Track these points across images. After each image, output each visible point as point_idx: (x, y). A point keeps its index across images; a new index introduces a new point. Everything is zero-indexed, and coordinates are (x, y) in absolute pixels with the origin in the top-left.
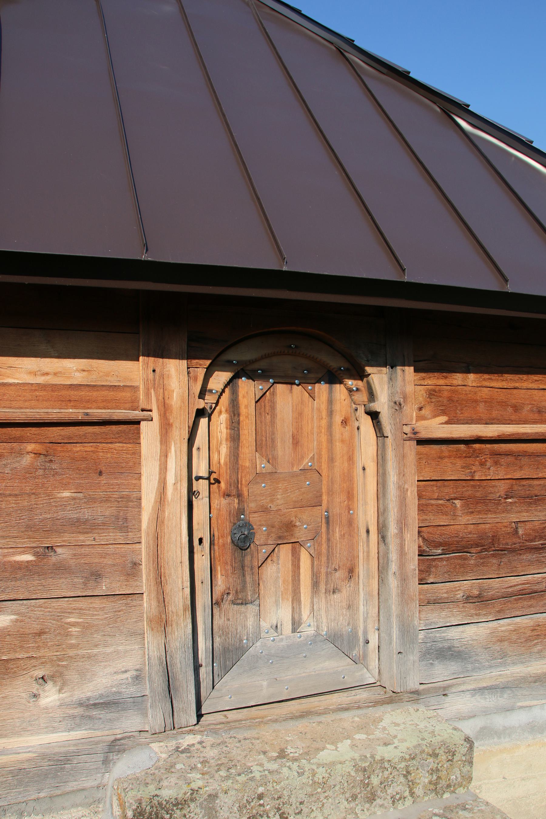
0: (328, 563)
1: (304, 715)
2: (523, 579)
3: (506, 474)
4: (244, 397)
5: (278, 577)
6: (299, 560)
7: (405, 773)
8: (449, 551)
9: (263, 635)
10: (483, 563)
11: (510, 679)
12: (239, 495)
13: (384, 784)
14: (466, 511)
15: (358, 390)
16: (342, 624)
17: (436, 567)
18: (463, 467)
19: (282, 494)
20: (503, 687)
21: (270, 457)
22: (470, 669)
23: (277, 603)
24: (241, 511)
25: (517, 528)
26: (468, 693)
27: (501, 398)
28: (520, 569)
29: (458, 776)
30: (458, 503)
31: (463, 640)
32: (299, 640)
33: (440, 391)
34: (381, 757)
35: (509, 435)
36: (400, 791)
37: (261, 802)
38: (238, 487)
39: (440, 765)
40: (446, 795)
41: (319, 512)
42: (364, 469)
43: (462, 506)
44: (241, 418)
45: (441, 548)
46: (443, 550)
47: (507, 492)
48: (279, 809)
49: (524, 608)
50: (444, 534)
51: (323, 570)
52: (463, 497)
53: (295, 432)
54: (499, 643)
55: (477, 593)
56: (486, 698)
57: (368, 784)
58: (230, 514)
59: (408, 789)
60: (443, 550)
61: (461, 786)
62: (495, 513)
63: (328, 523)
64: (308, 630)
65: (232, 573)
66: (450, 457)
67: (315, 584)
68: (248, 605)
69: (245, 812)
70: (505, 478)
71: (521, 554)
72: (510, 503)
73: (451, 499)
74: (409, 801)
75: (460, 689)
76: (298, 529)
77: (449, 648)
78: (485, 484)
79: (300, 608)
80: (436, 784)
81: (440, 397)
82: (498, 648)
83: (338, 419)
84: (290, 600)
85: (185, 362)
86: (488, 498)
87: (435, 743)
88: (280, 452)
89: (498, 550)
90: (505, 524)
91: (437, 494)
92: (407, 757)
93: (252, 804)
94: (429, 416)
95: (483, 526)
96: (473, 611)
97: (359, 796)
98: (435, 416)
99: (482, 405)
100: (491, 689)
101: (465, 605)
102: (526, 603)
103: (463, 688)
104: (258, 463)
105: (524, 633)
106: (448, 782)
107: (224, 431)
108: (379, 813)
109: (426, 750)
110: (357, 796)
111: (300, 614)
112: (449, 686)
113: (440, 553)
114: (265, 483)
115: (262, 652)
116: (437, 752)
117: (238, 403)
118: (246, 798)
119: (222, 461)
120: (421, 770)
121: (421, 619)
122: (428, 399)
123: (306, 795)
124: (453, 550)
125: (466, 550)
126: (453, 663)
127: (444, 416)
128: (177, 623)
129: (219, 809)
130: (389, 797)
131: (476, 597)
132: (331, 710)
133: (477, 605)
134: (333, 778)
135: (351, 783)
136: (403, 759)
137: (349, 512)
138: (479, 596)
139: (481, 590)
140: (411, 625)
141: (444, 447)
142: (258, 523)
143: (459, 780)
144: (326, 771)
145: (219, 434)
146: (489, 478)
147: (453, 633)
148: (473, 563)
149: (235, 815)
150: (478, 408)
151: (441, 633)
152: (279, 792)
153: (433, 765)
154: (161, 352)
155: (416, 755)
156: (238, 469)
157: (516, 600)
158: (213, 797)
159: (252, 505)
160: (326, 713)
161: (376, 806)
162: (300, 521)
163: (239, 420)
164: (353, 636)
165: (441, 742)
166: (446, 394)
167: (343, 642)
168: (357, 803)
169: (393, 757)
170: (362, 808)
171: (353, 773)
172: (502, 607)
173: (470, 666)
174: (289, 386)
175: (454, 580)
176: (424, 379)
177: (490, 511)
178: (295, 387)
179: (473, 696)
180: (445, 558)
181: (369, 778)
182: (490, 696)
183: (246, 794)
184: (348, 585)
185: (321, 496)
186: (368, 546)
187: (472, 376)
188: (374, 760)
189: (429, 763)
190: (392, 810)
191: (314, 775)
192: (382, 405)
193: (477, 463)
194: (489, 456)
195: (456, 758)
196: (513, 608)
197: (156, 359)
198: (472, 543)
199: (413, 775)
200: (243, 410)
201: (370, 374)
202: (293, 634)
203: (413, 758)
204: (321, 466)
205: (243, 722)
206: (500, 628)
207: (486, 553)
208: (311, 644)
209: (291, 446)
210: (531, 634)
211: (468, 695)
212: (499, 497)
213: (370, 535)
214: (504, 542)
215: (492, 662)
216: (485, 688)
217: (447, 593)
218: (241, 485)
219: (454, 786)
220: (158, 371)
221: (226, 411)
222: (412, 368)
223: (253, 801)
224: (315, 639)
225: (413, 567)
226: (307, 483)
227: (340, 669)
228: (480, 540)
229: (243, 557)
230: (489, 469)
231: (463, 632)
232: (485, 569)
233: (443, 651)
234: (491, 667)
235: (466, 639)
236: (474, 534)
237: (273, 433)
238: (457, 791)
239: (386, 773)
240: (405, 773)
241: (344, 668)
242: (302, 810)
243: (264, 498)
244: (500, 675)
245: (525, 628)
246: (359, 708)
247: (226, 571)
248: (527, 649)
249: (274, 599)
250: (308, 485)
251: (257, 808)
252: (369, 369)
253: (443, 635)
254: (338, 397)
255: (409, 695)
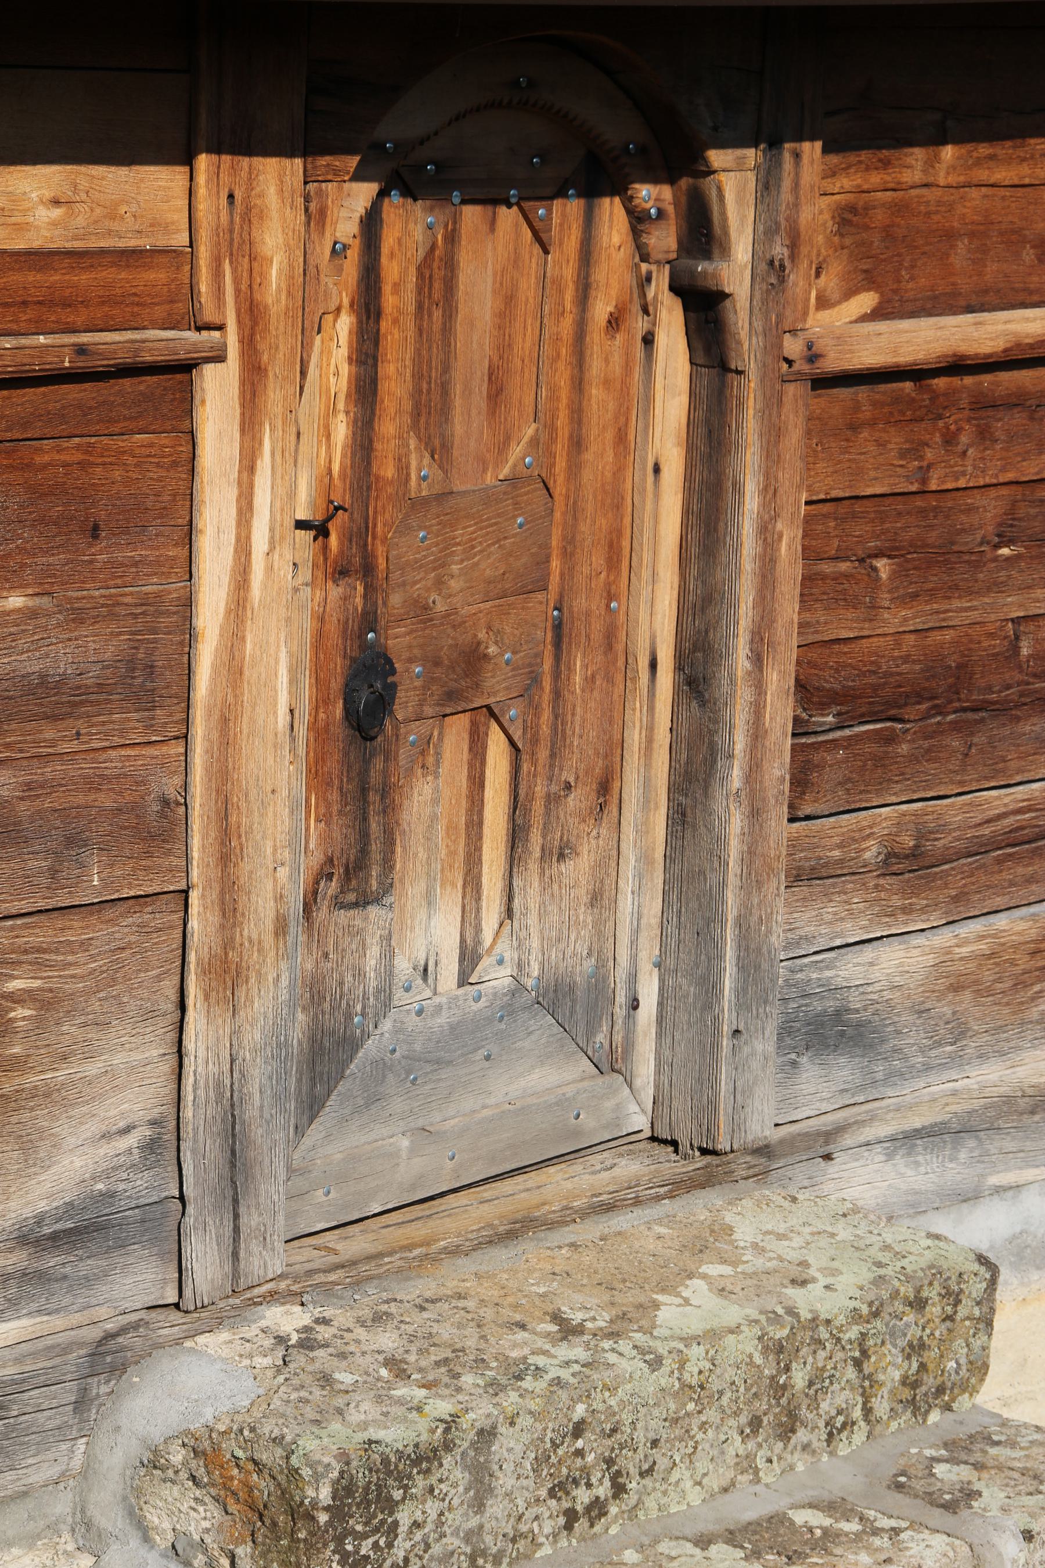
0: (552, 766)
1: (518, 1229)
2: (1020, 797)
3: (1003, 469)
4: (392, 255)
5: (434, 818)
6: (483, 763)
7: (857, 1354)
8: (853, 718)
9: (399, 996)
10: (928, 751)
11: (976, 1104)
12: (368, 570)
13: (818, 1383)
14: (902, 592)
15: (661, 214)
16: (576, 958)
17: (820, 767)
18: (902, 455)
19: (462, 561)
20: (959, 1128)
21: (437, 442)
22: (880, 1076)
23: (429, 900)
24: (369, 620)
25: (1017, 638)
26: (878, 1148)
27: (1010, 218)
28: (1013, 765)
29: (963, 1361)
30: (883, 566)
31: (870, 989)
32: (476, 1006)
33: (866, 208)
34: (811, 1311)
35: (1031, 346)
36: (844, 1406)
37: (580, 1443)
38: (366, 545)
39: (928, 1331)
40: (934, 1416)
41: (539, 608)
42: (657, 470)
43: (894, 575)
44: (384, 325)
45: (835, 709)
46: (839, 714)
47: (1000, 525)
48: (610, 1462)
49: (1015, 885)
50: (846, 666)
51: (540, 790)
52: (897, 549)
53: (496, 359)
54: (950, 996)
55: (911, 844)
56: (917, 1164)
57: (784, 1387)
58: (345, 631)
59: (860, 1399)
60: (839, 714)
61: (964, 1391)
62: (970, 593)
63: (558, 643)
64: (496, 977)
65: (340, 812)
66: (872, 423)
67: (516, 835)
68: (370, 908)
69: (544, 1473)
70: (1001, 480)
71: (1018, 719)
72: (1008, 559)
73: (870, 556)
74: (859, 1436)
75: (862, 1139)
76: (491, 667)
77: (838, 1013)
78: (949, 504)
79: (478, 910)
80: (915, 1385)
81: (867, 228)
82: (947, 1011)
83: (601, 309)
84: (460, 884)
85: (298, 162)
86: (955, 548)
87: (915, 1271)
88: (458, 427)
89: (964, 710)
90: (991, 628)
91: (836, 543)
92: (865, 1310)
93: (560, 1452)
94: (836, 296)
95: (937, 637)
96: (897, 901)
97: (765, 1420)
98: (849, 294)
99: (962, 246)
100: (931, 1135)
101: (882, 881)
102: (1020, 870)
103: (869, 1133)
104: (414, 464)
105: (1013, 963)
106: (939, 1380)
107: (345, 369)
108: (800, 1467)
109: (902, 1289)
110: (761, 1421)
111: (478, 929)
112: (840, 1130)
113: (867, 715)
114: (425, 528)
115: (394, 1051)
116: (925, 1294)
117: (378, 276)
118: (549, 1435)
119: (336, 468)
120: (889, 1346)
121: (794, 922)
122: (836, 239)
123: (665, 1420)
124: (862, 715)
125: (892, 712)
126: (842, 1060)
127: (868, 290)
128: (259, 973)
129: (496, 1467)
130: (821, 1424)
131: (907, 857)
132: (576, 1212)
133: (908, 881)
134: (718, 1371)
135: (752, 1385)
136: (856, 1317)
137: (608, 606)
138: (915, 854)
139: (922, 835)
140: (765, 950)
141: (862, 393)
142: (405, 655)
143: (963, 1372)
144: (707, 1353)
145: (332, 380)
146: (962, 483)
147: (849, 969)
148: (905, 753)
149: (525, 1482)
150: (952, 259)
151: (821, 970)
152: (614, 1414)
153: (914, 1333)
154: (243, 140)
155: (882, 1305)
156: (369, 488)
157: (999, 861)
158: (487, 1435)
159: (396, 599)
160: (565, 1223)
161: (795, 1447)
162: (496, 643)
163: (378, 330)
164: (599, 988)
165: (930, 1267)
166: (880, 217)
167: (574, 1007)
168: (760, 1439)
169: (836, 1311)
170: (769, 1454)
171: (758, 1360)
172: (965, 885)
173: (880, 1069)
174: (489, 208)
175: (858, 806)
176: (834, 174)
177: (957, 588)
178: (503, 210)
179: (890, 1156)
180: (844, 738)
181: (787, 1369)
182: (928, 1157)
183: (550, 1425)
184: (594, 833)
185: (548, 560)
186: (651, 708)
187: (948, 152)
188: (799, 1321)
189: (907, 1325)
190: (825, 1458)
191: (682, 1367)
192: (736, 270)
193: (938, 438)
194: (967, 412)
195: (962, 1312)
196: (989, 887)
197: (237, 158)
198: (907, 689)
199: (873, 1359)
200: (389, 301)
201: (714, 172)
202: (461, 991)
203: (876, 1314)
204: (553, 465)
205: (386, 1260)
206: (957, 950)
207: (939, 718)
208: (502, 1017)
209: (484, 405)
210: (1027, 966)
211: (877, 1154)
212: (981, 544)
213: (659, 674)
214: (982, 683)
215: (933, 1053)
216: (917, 1134)
217: (840, 846)
218: (374, 538)
219: (952, 1389)
220: (238, 195)
221: (352, 305)
222: (818, 145)
223: (563, 1443)
224: (513, 1004)
225: (777, 773)
226: (519, 520)
227: (570, 1091)
228: (927, 679)
229: (367, 762)
230: (964, 453)
231: (872, 964)
232: (931, 767)
233: (822, 1025)
234: (928, 1068)
235: (877, 987)
236: (914, 662)
237: (446, 369)
238: (955, 1406)
239: (822, 1354)
240: (857, 1354)
241: (580, 1085)
242: (655, 1463)
243: (422, 575)
244: (954, 1093)
245: (1016, 947)
246: (637, 1202)
247: (328, 806)
248: (1014, 1013)
249: (423, 885)
250: (521, 526)
251: (569, 1462)
252: (717, 157)
253: (828, 974)
254: (605, 238)
255: (748, 1158)
